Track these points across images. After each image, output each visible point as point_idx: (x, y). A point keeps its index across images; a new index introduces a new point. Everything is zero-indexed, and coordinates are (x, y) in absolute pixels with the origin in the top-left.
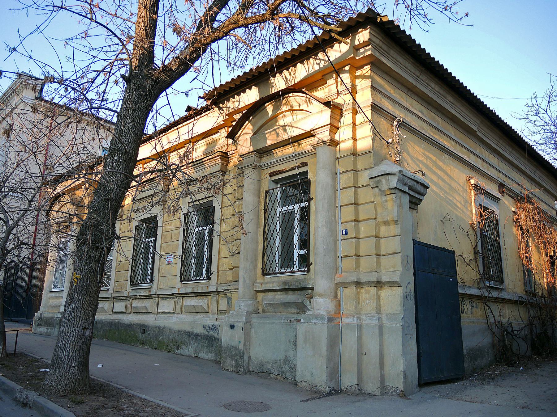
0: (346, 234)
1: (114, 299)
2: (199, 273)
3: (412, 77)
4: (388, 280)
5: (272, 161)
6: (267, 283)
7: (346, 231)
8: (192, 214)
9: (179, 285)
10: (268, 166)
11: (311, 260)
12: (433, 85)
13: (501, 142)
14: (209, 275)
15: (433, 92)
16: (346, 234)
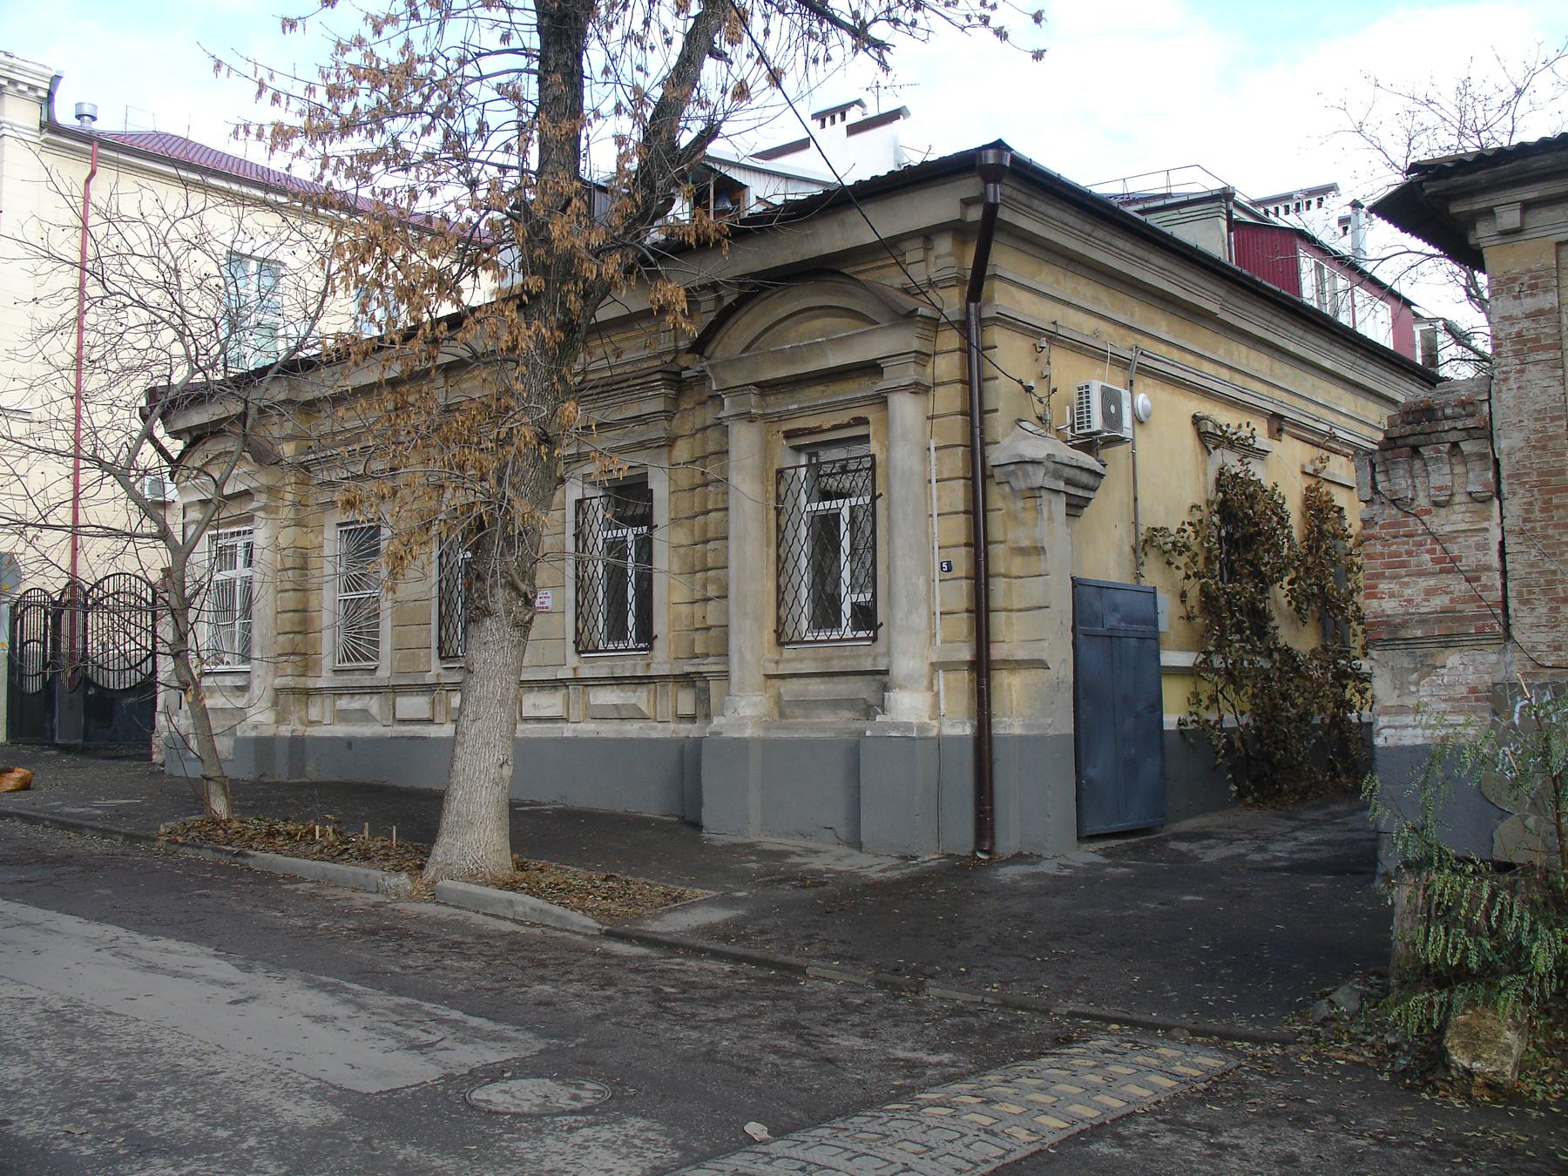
0: (949, 570)
1: (397, 690)
2: (617, 630)
3: (1077, 238)
4: (1026, 657)
5: (791, 407)
6: (789, 661)
7: (949, 564)
8: (595, 502)
9: (573, 660)
10: (782, 417)
11: (880, 618)
12: (1119, 243)
13: (1276, 321)
14: (646, 634)
15: (1119, 256)
16: (949, 570)
